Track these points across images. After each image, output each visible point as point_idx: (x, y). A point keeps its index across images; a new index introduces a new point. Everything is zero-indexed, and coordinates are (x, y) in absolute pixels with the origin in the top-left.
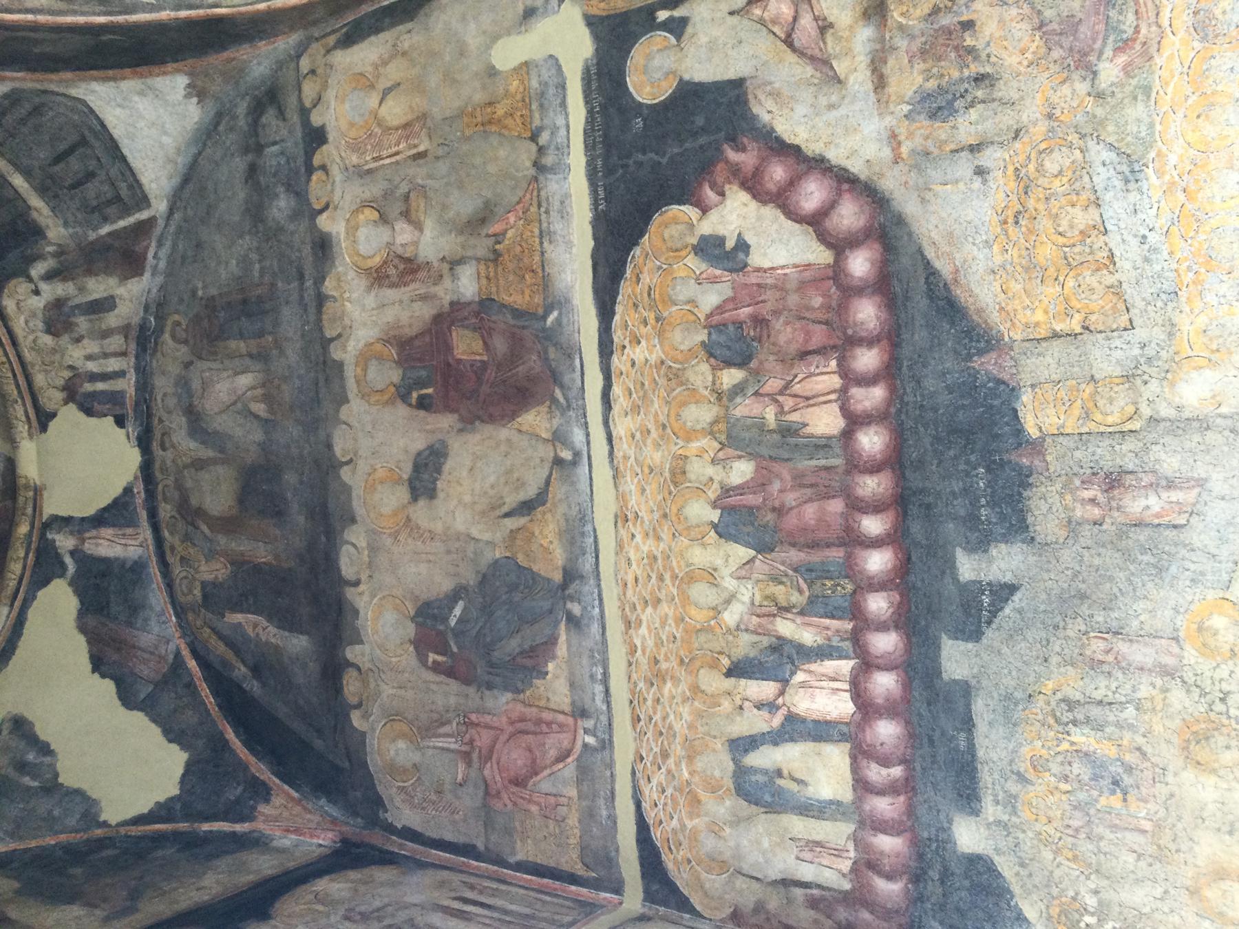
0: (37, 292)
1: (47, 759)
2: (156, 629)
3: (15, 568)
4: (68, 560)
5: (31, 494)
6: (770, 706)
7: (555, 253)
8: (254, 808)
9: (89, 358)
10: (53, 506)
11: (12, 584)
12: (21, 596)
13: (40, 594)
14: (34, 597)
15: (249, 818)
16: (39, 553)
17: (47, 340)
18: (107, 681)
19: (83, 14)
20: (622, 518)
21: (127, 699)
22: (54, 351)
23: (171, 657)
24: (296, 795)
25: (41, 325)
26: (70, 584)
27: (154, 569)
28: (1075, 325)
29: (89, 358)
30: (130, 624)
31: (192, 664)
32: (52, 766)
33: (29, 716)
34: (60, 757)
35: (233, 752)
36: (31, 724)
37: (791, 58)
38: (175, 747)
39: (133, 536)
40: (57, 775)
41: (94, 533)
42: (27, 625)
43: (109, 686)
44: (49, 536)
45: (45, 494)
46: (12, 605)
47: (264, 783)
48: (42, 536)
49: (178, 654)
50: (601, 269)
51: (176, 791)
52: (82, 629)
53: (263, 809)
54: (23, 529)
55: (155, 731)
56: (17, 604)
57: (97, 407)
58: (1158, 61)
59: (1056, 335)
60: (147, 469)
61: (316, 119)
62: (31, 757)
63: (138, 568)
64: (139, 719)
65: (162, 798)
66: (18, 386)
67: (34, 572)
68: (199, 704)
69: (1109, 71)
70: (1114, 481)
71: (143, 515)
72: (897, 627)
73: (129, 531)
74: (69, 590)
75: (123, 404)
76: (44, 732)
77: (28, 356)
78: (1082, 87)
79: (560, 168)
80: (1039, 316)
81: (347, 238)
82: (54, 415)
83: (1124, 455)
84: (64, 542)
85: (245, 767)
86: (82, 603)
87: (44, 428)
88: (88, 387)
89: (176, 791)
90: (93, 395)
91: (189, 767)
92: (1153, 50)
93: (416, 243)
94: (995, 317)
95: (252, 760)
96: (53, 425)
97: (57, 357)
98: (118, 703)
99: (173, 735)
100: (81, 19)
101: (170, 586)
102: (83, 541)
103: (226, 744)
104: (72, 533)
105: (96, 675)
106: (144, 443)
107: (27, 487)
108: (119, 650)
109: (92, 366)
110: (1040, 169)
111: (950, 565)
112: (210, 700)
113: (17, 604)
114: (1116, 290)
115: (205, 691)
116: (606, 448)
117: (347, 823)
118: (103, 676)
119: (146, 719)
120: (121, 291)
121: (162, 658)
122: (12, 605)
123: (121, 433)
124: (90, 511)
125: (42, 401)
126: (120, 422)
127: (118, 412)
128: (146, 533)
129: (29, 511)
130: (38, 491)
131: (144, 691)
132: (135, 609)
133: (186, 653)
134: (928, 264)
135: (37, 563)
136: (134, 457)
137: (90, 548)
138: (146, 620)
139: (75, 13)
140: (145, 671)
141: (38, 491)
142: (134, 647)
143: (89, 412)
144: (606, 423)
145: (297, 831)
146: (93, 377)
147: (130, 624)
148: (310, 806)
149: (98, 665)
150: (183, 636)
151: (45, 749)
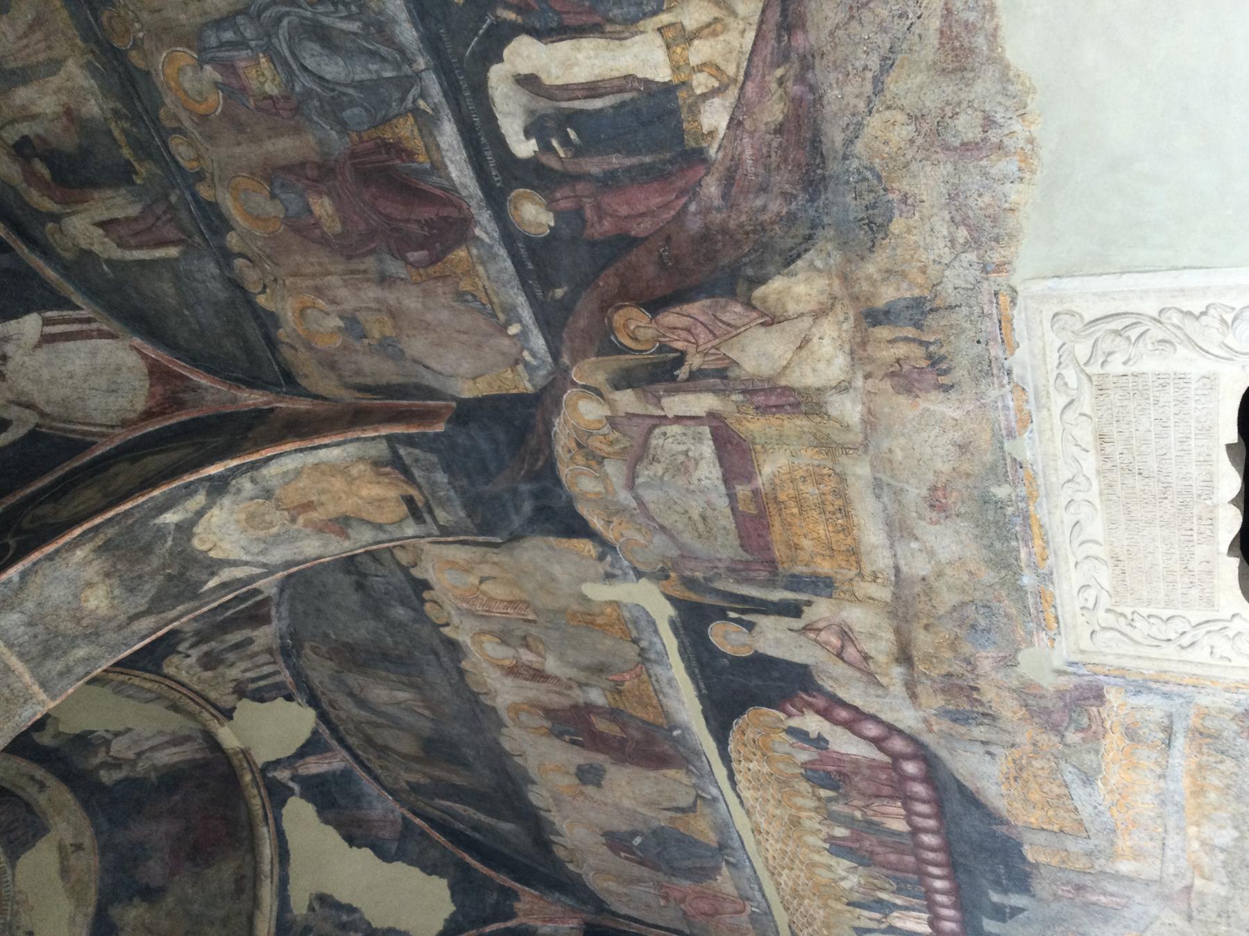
0: (188, 656)
1: (357, 916)
2: (380, 806)
3: (256, 802)
4: (291, 784)
5: (241, 756)
6: (879, 921)
7: (671, 704)
8: (512, 907)
9: (245, 671)
10: (262, 756)
11: (260, 812)
12: (270, 816)
13: (284, 811)
14: (281, 815)
15: (512, 915)
16: (267, 787)
17: (209, 674)
18: (364, 849)
19: (215, 600)
20: (756, 830)
21: (384, 855)
22: (215, 677)
23: (400, 820)
24: (536, 893)
25: (198, 669)
26: (302, 797)
27: (359, 771)
28: (1056, 828)
29: (245, 671)
30: (359, 808)
31: (417, 821)
32: (362, 919)
33: (328, 892)
34: (363, 910)
35: (475, 870)
36: (331, 896)
37: (841, 663)
38: (435, 878)
39: (334, 757)
40: (369, 924)
41: (301, 762)
42: (287, 833)
43: (367, 852)
44: (270, 775)
45: (252, 752)
46: (267, 825)
47: (509, 889)
48: (264, 777)
49: (404, 818)
50: (712, 722)
51: (452, 908)
52: (326, 822)
53: (518, 906)
54: (248, 778)
55: (415, 871)
56: (271, 821)
57: (266, 696)
58: (1104, 742)
59: (1043, 829)
60: (323, 716)
61: (416, 573)
62: (345, 918)
63: (346, 775)
64: (399, 867)
65: (446, 916)
66: (197, 703)
67: (271, 802)
68: (434, 844)
69: (1073, 737)
70: (1079, 888)
71: (334, 743)
72: (945, 852)
73: (328, 754)
74: (303, 801)
75: (286, 688)
76: (343, 897)
77: (197, 688)
78: (1056, 739)
79: (662, 659)
80: (1033, 820)
81: (474, 643)
82: (234, 708)
83: (1087, 880)
84: (283, 775)
85: (492, 880)
86: (315, 804)
87: (231, 718)
88: (252, 686)
89: (452, 908)
90: (259, 689)
91: (452, 887)
92: (1100, 737)
93: (543, 664)
94: (1005, 813)
95: (492, 874)
96: (235, 715)
97: (220, 679)
98: (379, 861)
99: (430, 869)
100: (215, 604)
101: (376, 779)
102: (296, 769)
103: (468, 867)
104: (285, 768)
105: (354, 848)
106: (313, 701)
107: (236, 753)
108: (360, 826)
109: (249, 675)
110: (1029, 763)
111: (987, 895)
112: (442, 839)
113: (271, 821)
114: (1080, 822)
115: (436, 835)
116: (737, 800)
117: (583, 911)
118: (359, 847)
119: (404, 865)
120: (256, 633)
121: (393, 822)
122: (267, 825)
123: (294, 705)
124: (292, 751)
125: (221, 704)
126: (289, 698)
127: (285, 693)
128: (344, 753)
129: (245, 765)
130: (245, 753)
131: (394, 847)
132: (358, 799)
133: (409, 815)
134: (958, 781)
135: (270, 794)
136: (310, 715)
137: (302, 771)
138: (370, 803)
139: (208, 603)
140: (386, 834)
141: (245, 753)
142: (370, 821)
143: (262, 700)
144: (734, 789)
145: (551, 920)
146: (253, 680)
147: (359, 808)
148: (550, 899)
149: (351, 841)
150: (402, 806)
151: (351, 909)
